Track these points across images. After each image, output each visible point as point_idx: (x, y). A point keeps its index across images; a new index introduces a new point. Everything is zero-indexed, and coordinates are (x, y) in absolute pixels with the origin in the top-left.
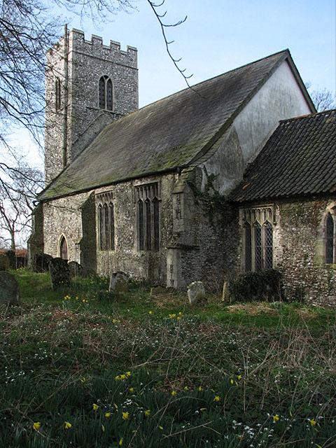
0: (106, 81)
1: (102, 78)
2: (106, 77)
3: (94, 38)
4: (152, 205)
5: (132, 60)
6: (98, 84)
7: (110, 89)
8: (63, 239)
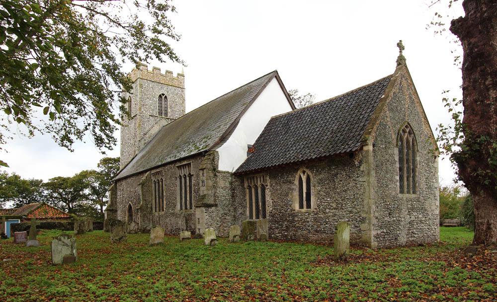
0: (163, 97)
1: (160, 96)
2: (163, 95)
3: (167, 72)
4: (188, 178)
5: (181, 83)
6: (157, 100)
7: (166, 103)
8: (130, 206)
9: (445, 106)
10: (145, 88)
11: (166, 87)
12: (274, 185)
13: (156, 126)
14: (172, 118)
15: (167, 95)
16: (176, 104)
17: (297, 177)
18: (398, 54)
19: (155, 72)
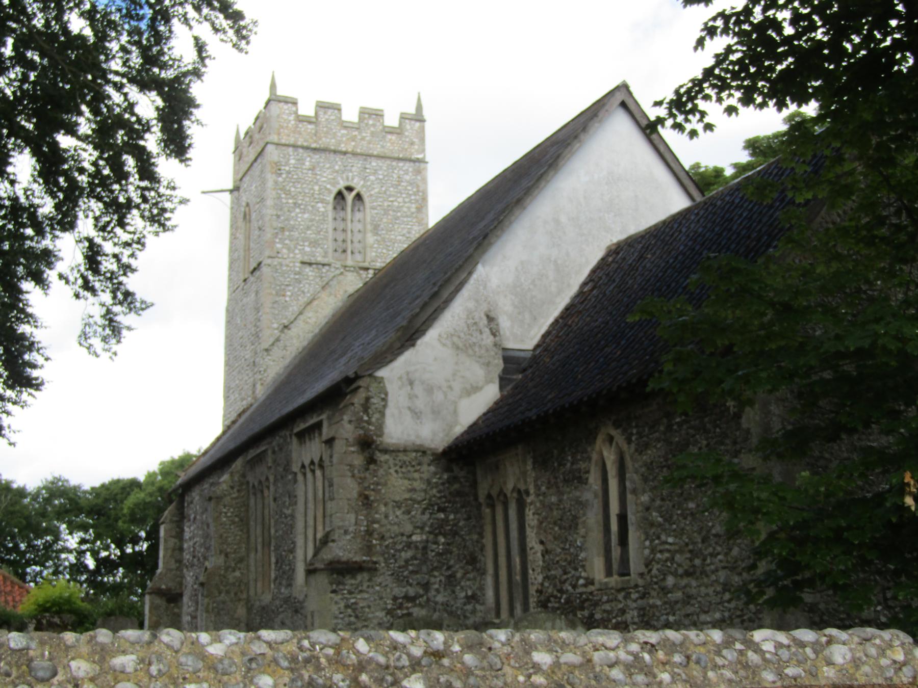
0: (350, 197)
2: (350, 189)
6: (330, 207)
10: (289, 172)
11: (358, 164)
12: (543, 488)
13: (324, 295)
16: (397, 218)
19: (323, 118)
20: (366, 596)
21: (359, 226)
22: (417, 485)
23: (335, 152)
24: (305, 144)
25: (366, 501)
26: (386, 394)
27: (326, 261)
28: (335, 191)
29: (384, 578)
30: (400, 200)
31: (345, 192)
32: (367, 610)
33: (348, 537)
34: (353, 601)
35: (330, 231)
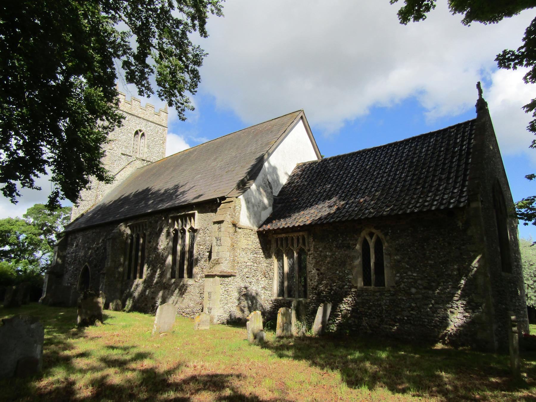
0: (140, 134)
2: (141, 131)
9: (40, 189)
11: (145, 122)
14: (148, 160)
15: (140, 129)
17: (360, 239)
18: (478, 98)
20: (231, 286)
21: (142, 145)
22: (250, 243)
23: (137, 117)
24: (127, 111)
25: (233, 247)
26: (241, 206)
27: (129, 154)
28: (135, 130)
29: (238, 279)
30: (157, 138)
31: (139, 132)
32: (231, 292)
33: (227, 262)
34: (227, 288)
35: (132, 144)
